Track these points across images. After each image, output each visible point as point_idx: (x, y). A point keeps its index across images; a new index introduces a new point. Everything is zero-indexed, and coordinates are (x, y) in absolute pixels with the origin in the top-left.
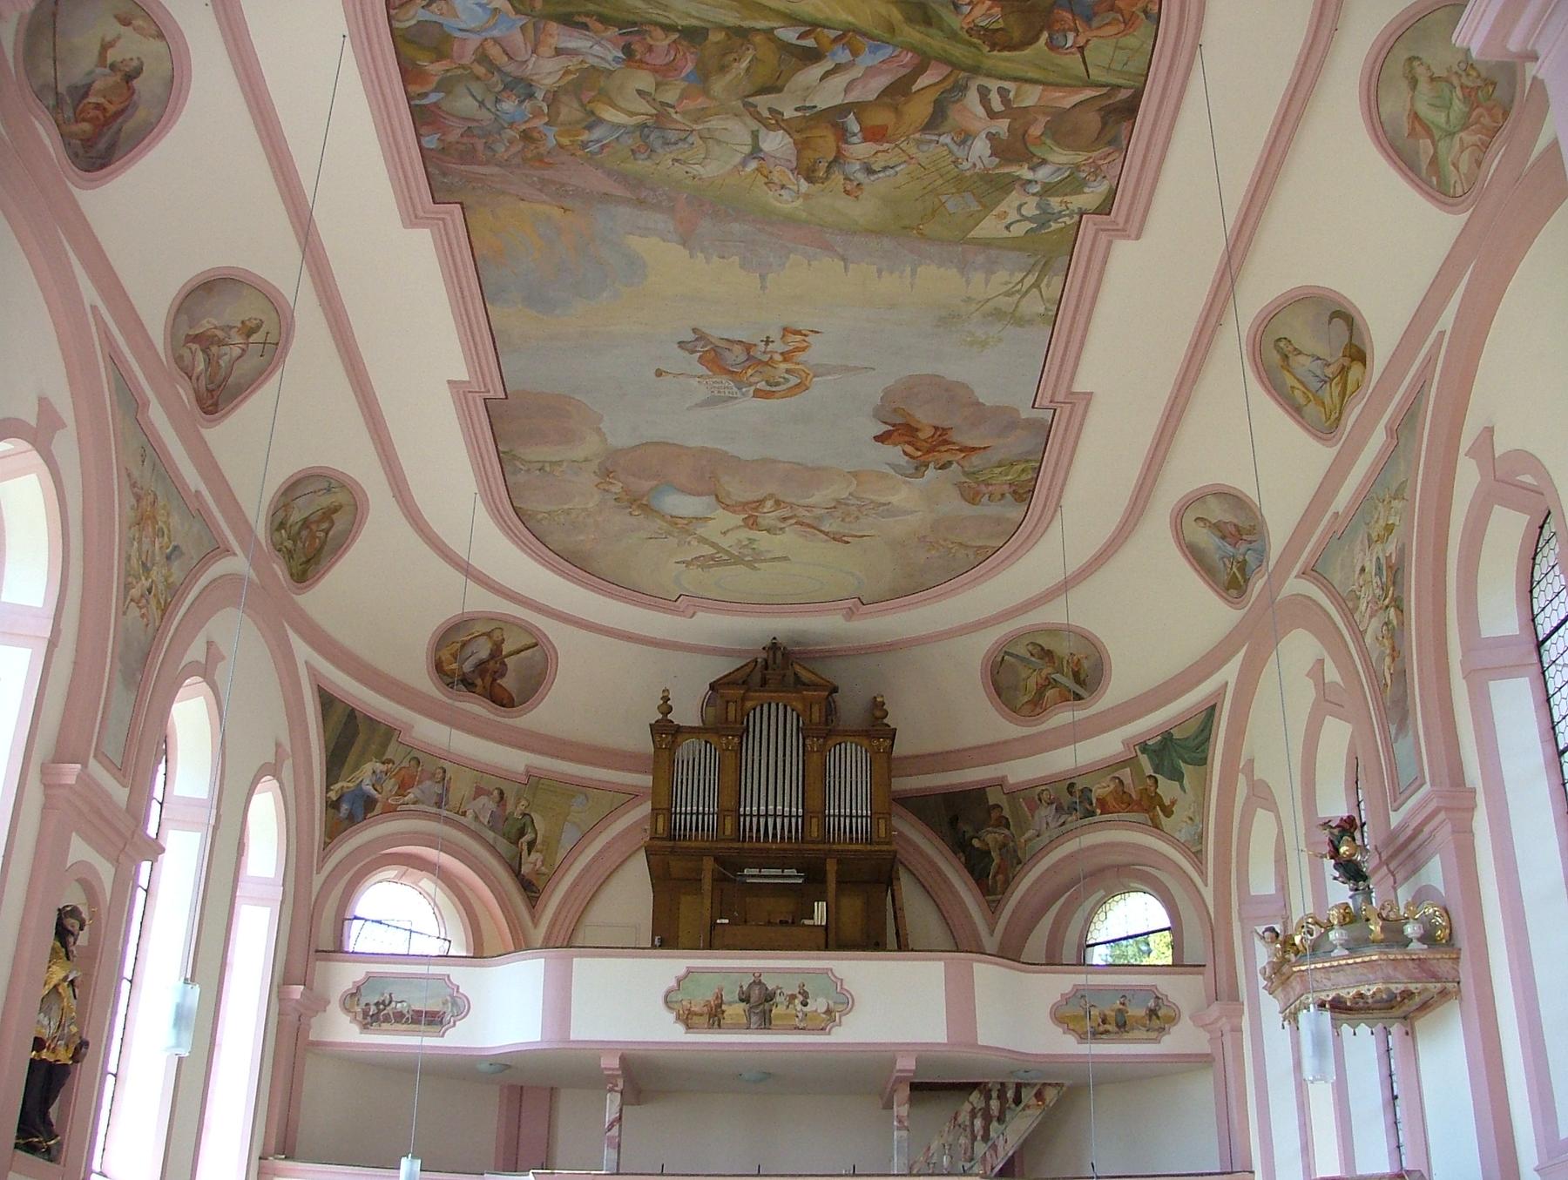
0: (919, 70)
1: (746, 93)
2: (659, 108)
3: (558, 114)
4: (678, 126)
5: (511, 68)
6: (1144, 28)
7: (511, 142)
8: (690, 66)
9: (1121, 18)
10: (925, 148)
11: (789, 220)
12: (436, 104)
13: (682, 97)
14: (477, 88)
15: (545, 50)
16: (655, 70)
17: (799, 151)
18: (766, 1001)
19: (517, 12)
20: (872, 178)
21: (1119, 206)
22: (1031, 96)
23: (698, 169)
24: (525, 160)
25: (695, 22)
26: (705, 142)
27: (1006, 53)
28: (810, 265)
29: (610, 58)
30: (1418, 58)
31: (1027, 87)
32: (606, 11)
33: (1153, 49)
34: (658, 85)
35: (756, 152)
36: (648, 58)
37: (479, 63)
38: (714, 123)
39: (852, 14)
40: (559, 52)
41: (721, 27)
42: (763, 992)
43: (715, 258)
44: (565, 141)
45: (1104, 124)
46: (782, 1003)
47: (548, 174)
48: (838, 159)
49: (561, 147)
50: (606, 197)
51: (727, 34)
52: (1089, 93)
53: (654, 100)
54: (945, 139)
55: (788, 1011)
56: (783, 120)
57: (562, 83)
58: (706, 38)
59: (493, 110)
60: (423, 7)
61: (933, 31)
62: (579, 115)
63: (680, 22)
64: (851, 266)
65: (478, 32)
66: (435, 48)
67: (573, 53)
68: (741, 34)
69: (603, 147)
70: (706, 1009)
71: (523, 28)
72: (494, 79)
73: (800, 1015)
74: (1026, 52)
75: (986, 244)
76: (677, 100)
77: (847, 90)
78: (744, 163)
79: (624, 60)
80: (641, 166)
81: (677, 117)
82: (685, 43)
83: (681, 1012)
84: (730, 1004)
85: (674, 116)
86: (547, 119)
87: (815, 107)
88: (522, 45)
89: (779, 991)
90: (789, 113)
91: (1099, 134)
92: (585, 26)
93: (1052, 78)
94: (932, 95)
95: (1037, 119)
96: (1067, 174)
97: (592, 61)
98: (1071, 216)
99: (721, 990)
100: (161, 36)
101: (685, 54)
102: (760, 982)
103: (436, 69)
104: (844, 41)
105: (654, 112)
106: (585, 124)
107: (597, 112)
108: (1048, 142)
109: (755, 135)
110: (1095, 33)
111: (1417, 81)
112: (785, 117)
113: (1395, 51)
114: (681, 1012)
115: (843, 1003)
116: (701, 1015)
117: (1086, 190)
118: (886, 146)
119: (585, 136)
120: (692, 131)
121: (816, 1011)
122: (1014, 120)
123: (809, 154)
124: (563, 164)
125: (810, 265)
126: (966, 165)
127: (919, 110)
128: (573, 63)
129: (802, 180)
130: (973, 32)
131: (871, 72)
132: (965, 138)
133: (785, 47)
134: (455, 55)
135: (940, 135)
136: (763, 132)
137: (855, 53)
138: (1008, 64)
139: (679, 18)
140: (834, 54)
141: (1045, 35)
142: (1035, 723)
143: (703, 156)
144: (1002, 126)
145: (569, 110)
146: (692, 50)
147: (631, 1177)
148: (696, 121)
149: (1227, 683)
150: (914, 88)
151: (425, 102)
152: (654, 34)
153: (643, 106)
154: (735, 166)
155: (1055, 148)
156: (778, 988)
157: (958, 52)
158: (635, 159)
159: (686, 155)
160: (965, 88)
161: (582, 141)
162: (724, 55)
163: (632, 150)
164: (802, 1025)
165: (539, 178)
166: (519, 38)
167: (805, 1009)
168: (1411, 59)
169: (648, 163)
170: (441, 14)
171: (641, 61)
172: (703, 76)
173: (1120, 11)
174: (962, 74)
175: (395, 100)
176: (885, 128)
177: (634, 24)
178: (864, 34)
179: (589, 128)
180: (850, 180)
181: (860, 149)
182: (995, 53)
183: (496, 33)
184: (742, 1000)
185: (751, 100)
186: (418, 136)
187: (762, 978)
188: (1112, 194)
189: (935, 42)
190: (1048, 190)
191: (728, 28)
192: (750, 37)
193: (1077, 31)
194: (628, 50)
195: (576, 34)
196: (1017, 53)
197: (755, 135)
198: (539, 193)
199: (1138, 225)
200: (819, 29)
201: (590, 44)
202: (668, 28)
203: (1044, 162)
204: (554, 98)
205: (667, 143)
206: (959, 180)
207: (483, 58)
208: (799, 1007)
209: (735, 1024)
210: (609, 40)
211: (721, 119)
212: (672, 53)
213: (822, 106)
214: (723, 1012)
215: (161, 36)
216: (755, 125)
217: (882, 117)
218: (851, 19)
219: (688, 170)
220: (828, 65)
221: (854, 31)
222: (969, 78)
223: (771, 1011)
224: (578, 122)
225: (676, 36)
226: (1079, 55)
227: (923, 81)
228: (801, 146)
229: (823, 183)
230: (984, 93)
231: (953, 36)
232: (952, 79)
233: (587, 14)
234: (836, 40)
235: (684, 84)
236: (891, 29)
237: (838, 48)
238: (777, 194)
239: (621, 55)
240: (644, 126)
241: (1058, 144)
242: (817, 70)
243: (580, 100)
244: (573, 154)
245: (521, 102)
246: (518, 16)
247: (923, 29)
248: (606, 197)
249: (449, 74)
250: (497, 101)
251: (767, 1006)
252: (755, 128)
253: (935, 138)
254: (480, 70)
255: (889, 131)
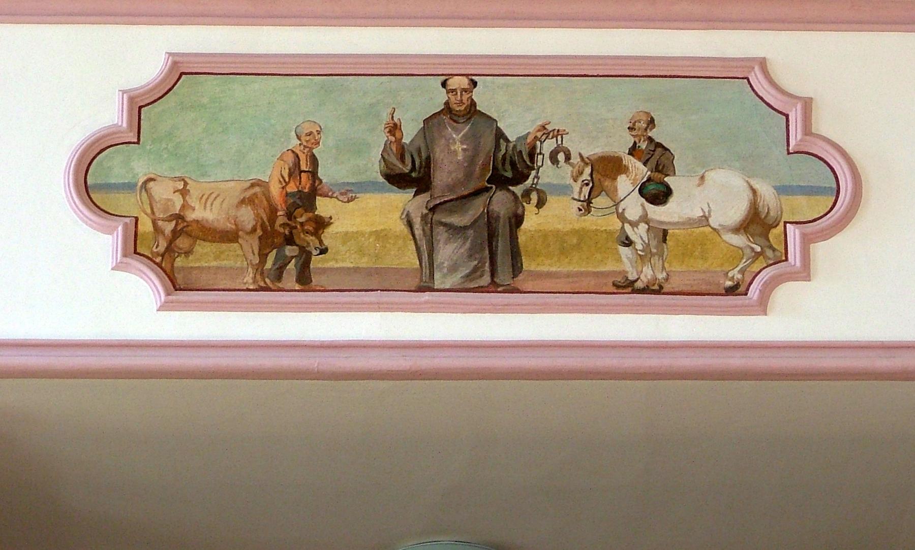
18: (499, 181)
42: (488, 142)
46: (563, 190)
55: (592, 221)
70: (247, 217)
73: (639, 235)
83: (146, 226)
84: (349, 193)
89: (548, 146)
99: (310, 139)
102: (472, 111)
114: (146, 226)
115: (811, 191)
116: (229, 236)
121: (705, 220)
147: (521, 74)
149: (420, 148)
156: (545, 132)
164: (647, 274)
167: (656, 212)
184: (396, 179)
187: (476, 95)
199: (521, 60)
208: (634, 206)
209: (370, 272)
214: (321, 224)
223: (517, 220)
251: (500, 202)
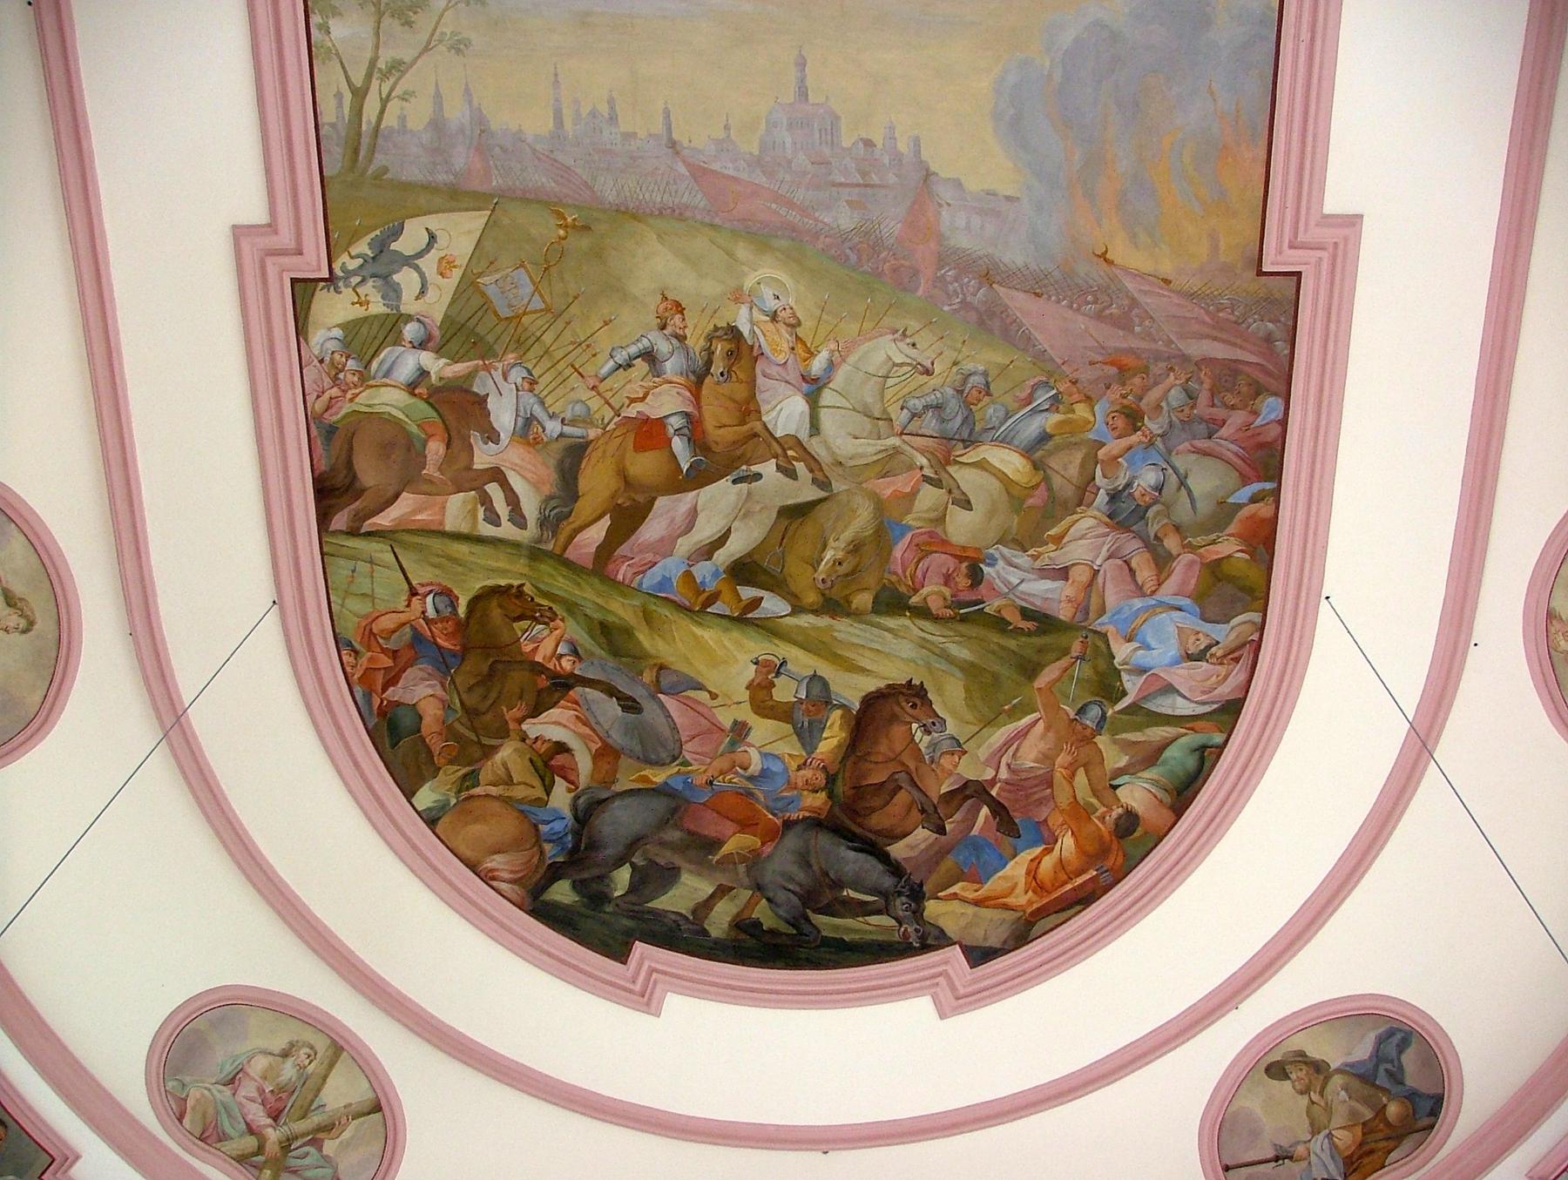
0: (606, 551)
1: (825, 506)
2: (944, 476)
3: (1082, 465)
4: (919, 441)
5: (1131, 546)
6: (350, 629)
7: (1158, 407)
8: (898, 552)
9: (381, 641)
10: (579, 409)
11: (761, 237)
12: (1245, 481)
13: (914, 494)
14: (1183, 512)
15: (1080, 575)
16: (944, 544)
17: (753, 396)
19: (1104, 636)
20: (645, 341)
21: (285, 315)
22: (456, 510)
23: (895, 351)
24: (1145, 370)
25: (891, 622)
26: (885, 411)
27: (503, 582)
28: (727, 127)
29: (1001, 563)
30: (24, 632)
31: (464, 528)
32: (995, 638)
33: (328, 599)
34: (941, 520)
35: (814, 388)
36: (951, 563)
37: (1170, 554)
38: (871, 450)
39: (694, 635)
40: (1063, 573)
41: (856, 615)
43: (878, 139)
44: (1081, 411)
45: (349, 464)
47: (1117, 340)
48: (698, 378)
49: (1088, 399)
50: (1037, 286)
51: (849, 603)
52: (384, 520)
53: (950, 492)
54: (553, 428)
56: (776, 457)
57: (1069, 519)
58: (876, 598)
59: (1170, 471)
60: (1218, 643)
61: (597, 616)
62: (1054, 463)
63: (907, 622)
64: (658, 127)
65: (1161, 603)
66: (1220, 580)
67: (1045, 573)
68: (833, 606)
69: (1029, 400)
71: (1102, 611)
72: (1156, 527)
74: (478, 587)
75: (455, 197)
76: (918, 491)
77: (693, 513)
78: (831, 366)
79: (983, 561)
80: (983, 358)
81: (922, 460)
82: (903, 589)
85: (924, 461)
86: (1101, 453)
87: (734, 482)
88: (1109, 585)
90: (768, 468)
91: (351, 448)
92: (1026, 614)
93: (436, 544)
94: (584, 508)
95: (440, 469)
96: (375, 365)
97: (1023, 559)
98: (349, 274)
100: (1551, 615)
101: (904, 572)
103: (1228, 547)
104: (706, 595)
105: (951, 469)
106: (1050, 445)
107: (1029, 467)
108: (414, 429)
109: (815, 428)
110: (403, 618)
111: (9, 605)
112: (774, 461)
113: (53, 627)
117: (338, 333)
118: (632, 412)
119: (1055, 418)
120: (902, 434)
122: (469, 468)
123: (740, 392)
124: (1092, 363)
125: (727, 127)
126: (517, 375)
127: (597, 481)
128: (1051, 555)
129: (746, 333)
130: (548, 614)
131: (665, 547)
132: (527, 429)
133: (777, 585)
134: (1197, 568)
135: (561, 435)
136: (803, 435)
137: (688, 575)
138: (495, 564)
139: (908, 627)
140: (716, 574)
141: (462, 611)
142: (227, 994)
143: (890, 382)
144: (483, 456)
145: (1067, 467)
146: (894, 578)
148: (897, 451)
150: (606, 522)
151: (1256, 487)
152: (941, 603)
153: (966, 478)
154: (844, 361)
155: (402, 416)
157: (561, 584)
158: (985, 374)
159: (913, 385)
160: (543, 523)
161: (1057, 411)
162: (853, 572)
163: (988, 394)
165: (1132, 331)
166: (1111, 600)
168: (31, 623)
169: (968, 366)
170: (1198, 633)
171: (961, 559)
172: (882, 535)
173: (384, 651)
174: (550, 547)
175: (1296, 486)
176: (639, 447)
177: (964, 619)
178: (679, 607)
179: (1044, 437)
180: (676, 336)
181: (667, 403)
182: (516, 583)
183: (1138, 603)
185: (822, 494)
186: (1284, 423)
188: (301, 330)
189: (588, 594)
190: (390, 328)
191: (848, 615)
192: (821, 599)
193: (428, 621)
194: (976, 576)
195: (1038, 603)
196: (490, 583)
197: (815, 428)
198: (1142, 299)
200: (736, 614)
201: (1022, 587)
202: (923, 612)
203: (411, 388)
204: (1084, 491)
205: (938, 407)
206: (521, 344)
207: (1162, 562)
210: (1000, 595)
211: (862, 456)
212: (919, 573)
213: (725, 483)
215: (1551, 615)
216: (815, 447)
217: (644, 465)
218: (698, 631)
219: (912, 352)
220: (723, 556)
221: (694, 612)
222: (539, 541)
224: (1058, 448)
225: (914, 600)
226: (414, 583)
227: (596, 534)
228: (748, 409)
229: (716, 329)
230: (518, 518)
231: (572, 608)
232: (562, 538)
233: (1019, 632)
234: (713, 598)
235: (909, 520)
236: (648, 617)
237: (711, 587)
238: (783, 301)
239: (986, 569)
240: (970, 443)
241: (397, 423)
242: (736, 547)
243: (1049, 489)
244: (1074, 383)
245: (1128, 485)
246: (1102, 629)
247: (611, 619)
248: (1037, 286)
249: (1213, 537)
250: (1159, 488)
252: (814, 440)
253: (568, 430)
254: (1171, 543)
255: (631, 438)
